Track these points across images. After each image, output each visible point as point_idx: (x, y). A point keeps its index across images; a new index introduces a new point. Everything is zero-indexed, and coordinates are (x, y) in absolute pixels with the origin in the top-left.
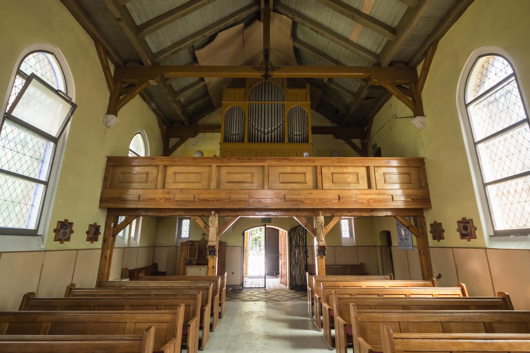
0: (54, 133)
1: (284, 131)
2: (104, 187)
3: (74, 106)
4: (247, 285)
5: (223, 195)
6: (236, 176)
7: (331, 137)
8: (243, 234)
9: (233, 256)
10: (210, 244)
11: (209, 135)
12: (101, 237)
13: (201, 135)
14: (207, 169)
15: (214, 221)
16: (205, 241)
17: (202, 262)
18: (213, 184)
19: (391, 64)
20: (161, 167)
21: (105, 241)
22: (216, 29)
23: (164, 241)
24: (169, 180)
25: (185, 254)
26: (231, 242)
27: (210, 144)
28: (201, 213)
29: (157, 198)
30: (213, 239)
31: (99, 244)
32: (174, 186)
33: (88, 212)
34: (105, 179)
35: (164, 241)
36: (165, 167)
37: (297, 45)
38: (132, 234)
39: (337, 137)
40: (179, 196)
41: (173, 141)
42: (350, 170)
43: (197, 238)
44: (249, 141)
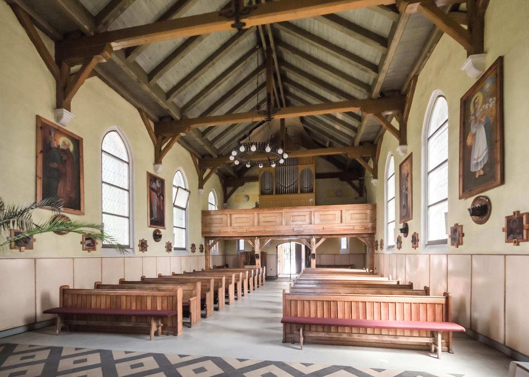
0: (184, 207)
1: (297, 185)
2: (203, 227)
3: (190, 192)
4: (279, 276)
5: (261, 229)
6: (268, 218)
7: (337, 180)
8: (277, 247)
9: (271, 260)
10: (256, 253)
11: (252, 183)
12: (204, 250)
13: (247, 184)
14: (252, 215)
15: (257, 242)
16: (254, 251)
17: (253, 263)
18: (256, 223)
19: (361, 144)
20: (229, 215)
21: (206, 252)
22: (252, 128)
23: (230, 252)
24: (233, 222)
25: (243, 258)
26: (270, 252)
27: (253, 190)
28: (250, 238)
29: (229, 231)
30: (257, 251)
31: (204, 253)
32: (236, 225)
33: (199, 241)
34: (202, 222)
35: (230, 252)
36: (231, 215)
37: (305, 126)
38: (216, 249)
39: (342, 179)
40: (239, 230)
41: (229, 189)
42: (331, 212)
43: (249, 250)
44: (277, 193)
